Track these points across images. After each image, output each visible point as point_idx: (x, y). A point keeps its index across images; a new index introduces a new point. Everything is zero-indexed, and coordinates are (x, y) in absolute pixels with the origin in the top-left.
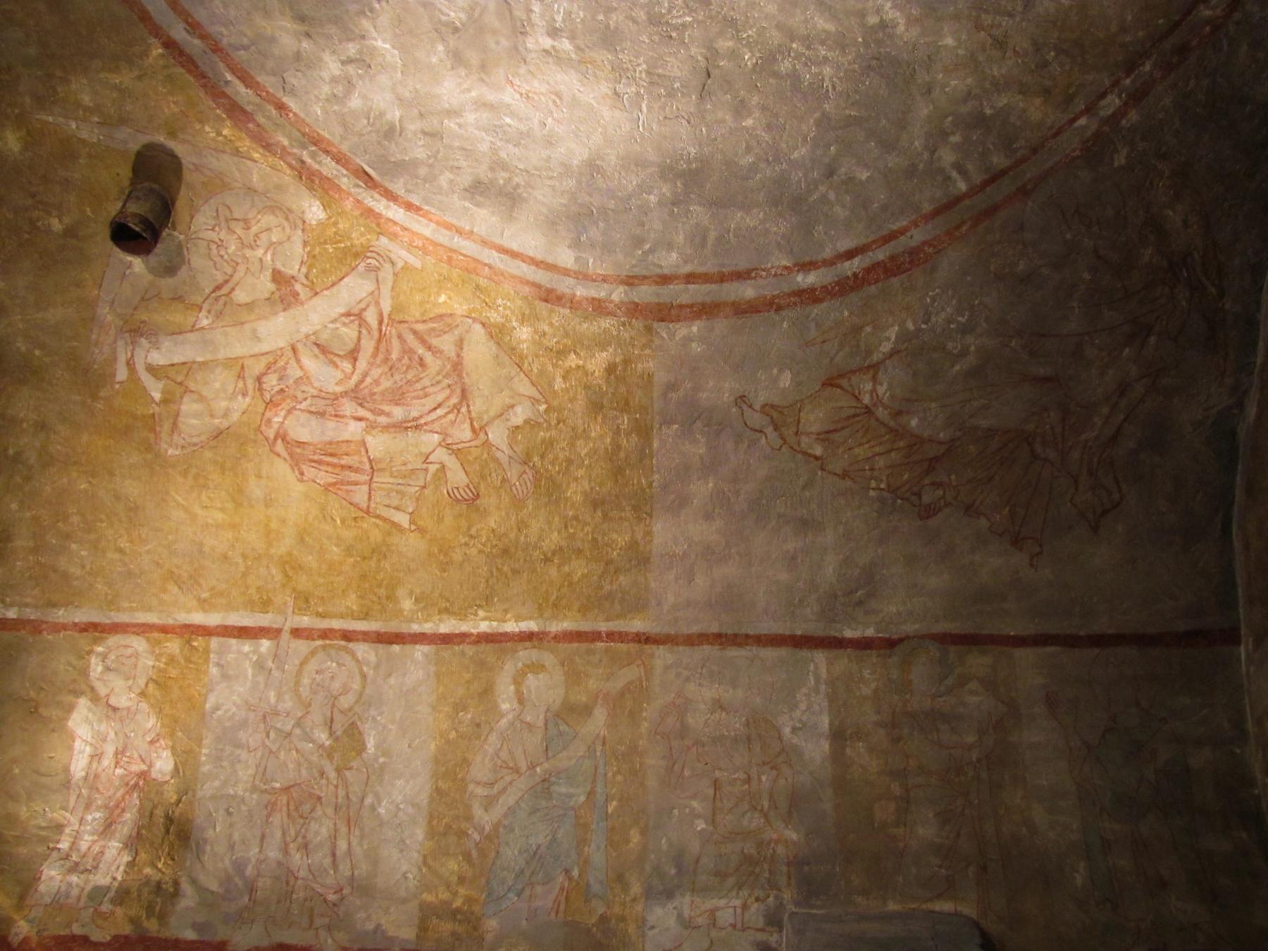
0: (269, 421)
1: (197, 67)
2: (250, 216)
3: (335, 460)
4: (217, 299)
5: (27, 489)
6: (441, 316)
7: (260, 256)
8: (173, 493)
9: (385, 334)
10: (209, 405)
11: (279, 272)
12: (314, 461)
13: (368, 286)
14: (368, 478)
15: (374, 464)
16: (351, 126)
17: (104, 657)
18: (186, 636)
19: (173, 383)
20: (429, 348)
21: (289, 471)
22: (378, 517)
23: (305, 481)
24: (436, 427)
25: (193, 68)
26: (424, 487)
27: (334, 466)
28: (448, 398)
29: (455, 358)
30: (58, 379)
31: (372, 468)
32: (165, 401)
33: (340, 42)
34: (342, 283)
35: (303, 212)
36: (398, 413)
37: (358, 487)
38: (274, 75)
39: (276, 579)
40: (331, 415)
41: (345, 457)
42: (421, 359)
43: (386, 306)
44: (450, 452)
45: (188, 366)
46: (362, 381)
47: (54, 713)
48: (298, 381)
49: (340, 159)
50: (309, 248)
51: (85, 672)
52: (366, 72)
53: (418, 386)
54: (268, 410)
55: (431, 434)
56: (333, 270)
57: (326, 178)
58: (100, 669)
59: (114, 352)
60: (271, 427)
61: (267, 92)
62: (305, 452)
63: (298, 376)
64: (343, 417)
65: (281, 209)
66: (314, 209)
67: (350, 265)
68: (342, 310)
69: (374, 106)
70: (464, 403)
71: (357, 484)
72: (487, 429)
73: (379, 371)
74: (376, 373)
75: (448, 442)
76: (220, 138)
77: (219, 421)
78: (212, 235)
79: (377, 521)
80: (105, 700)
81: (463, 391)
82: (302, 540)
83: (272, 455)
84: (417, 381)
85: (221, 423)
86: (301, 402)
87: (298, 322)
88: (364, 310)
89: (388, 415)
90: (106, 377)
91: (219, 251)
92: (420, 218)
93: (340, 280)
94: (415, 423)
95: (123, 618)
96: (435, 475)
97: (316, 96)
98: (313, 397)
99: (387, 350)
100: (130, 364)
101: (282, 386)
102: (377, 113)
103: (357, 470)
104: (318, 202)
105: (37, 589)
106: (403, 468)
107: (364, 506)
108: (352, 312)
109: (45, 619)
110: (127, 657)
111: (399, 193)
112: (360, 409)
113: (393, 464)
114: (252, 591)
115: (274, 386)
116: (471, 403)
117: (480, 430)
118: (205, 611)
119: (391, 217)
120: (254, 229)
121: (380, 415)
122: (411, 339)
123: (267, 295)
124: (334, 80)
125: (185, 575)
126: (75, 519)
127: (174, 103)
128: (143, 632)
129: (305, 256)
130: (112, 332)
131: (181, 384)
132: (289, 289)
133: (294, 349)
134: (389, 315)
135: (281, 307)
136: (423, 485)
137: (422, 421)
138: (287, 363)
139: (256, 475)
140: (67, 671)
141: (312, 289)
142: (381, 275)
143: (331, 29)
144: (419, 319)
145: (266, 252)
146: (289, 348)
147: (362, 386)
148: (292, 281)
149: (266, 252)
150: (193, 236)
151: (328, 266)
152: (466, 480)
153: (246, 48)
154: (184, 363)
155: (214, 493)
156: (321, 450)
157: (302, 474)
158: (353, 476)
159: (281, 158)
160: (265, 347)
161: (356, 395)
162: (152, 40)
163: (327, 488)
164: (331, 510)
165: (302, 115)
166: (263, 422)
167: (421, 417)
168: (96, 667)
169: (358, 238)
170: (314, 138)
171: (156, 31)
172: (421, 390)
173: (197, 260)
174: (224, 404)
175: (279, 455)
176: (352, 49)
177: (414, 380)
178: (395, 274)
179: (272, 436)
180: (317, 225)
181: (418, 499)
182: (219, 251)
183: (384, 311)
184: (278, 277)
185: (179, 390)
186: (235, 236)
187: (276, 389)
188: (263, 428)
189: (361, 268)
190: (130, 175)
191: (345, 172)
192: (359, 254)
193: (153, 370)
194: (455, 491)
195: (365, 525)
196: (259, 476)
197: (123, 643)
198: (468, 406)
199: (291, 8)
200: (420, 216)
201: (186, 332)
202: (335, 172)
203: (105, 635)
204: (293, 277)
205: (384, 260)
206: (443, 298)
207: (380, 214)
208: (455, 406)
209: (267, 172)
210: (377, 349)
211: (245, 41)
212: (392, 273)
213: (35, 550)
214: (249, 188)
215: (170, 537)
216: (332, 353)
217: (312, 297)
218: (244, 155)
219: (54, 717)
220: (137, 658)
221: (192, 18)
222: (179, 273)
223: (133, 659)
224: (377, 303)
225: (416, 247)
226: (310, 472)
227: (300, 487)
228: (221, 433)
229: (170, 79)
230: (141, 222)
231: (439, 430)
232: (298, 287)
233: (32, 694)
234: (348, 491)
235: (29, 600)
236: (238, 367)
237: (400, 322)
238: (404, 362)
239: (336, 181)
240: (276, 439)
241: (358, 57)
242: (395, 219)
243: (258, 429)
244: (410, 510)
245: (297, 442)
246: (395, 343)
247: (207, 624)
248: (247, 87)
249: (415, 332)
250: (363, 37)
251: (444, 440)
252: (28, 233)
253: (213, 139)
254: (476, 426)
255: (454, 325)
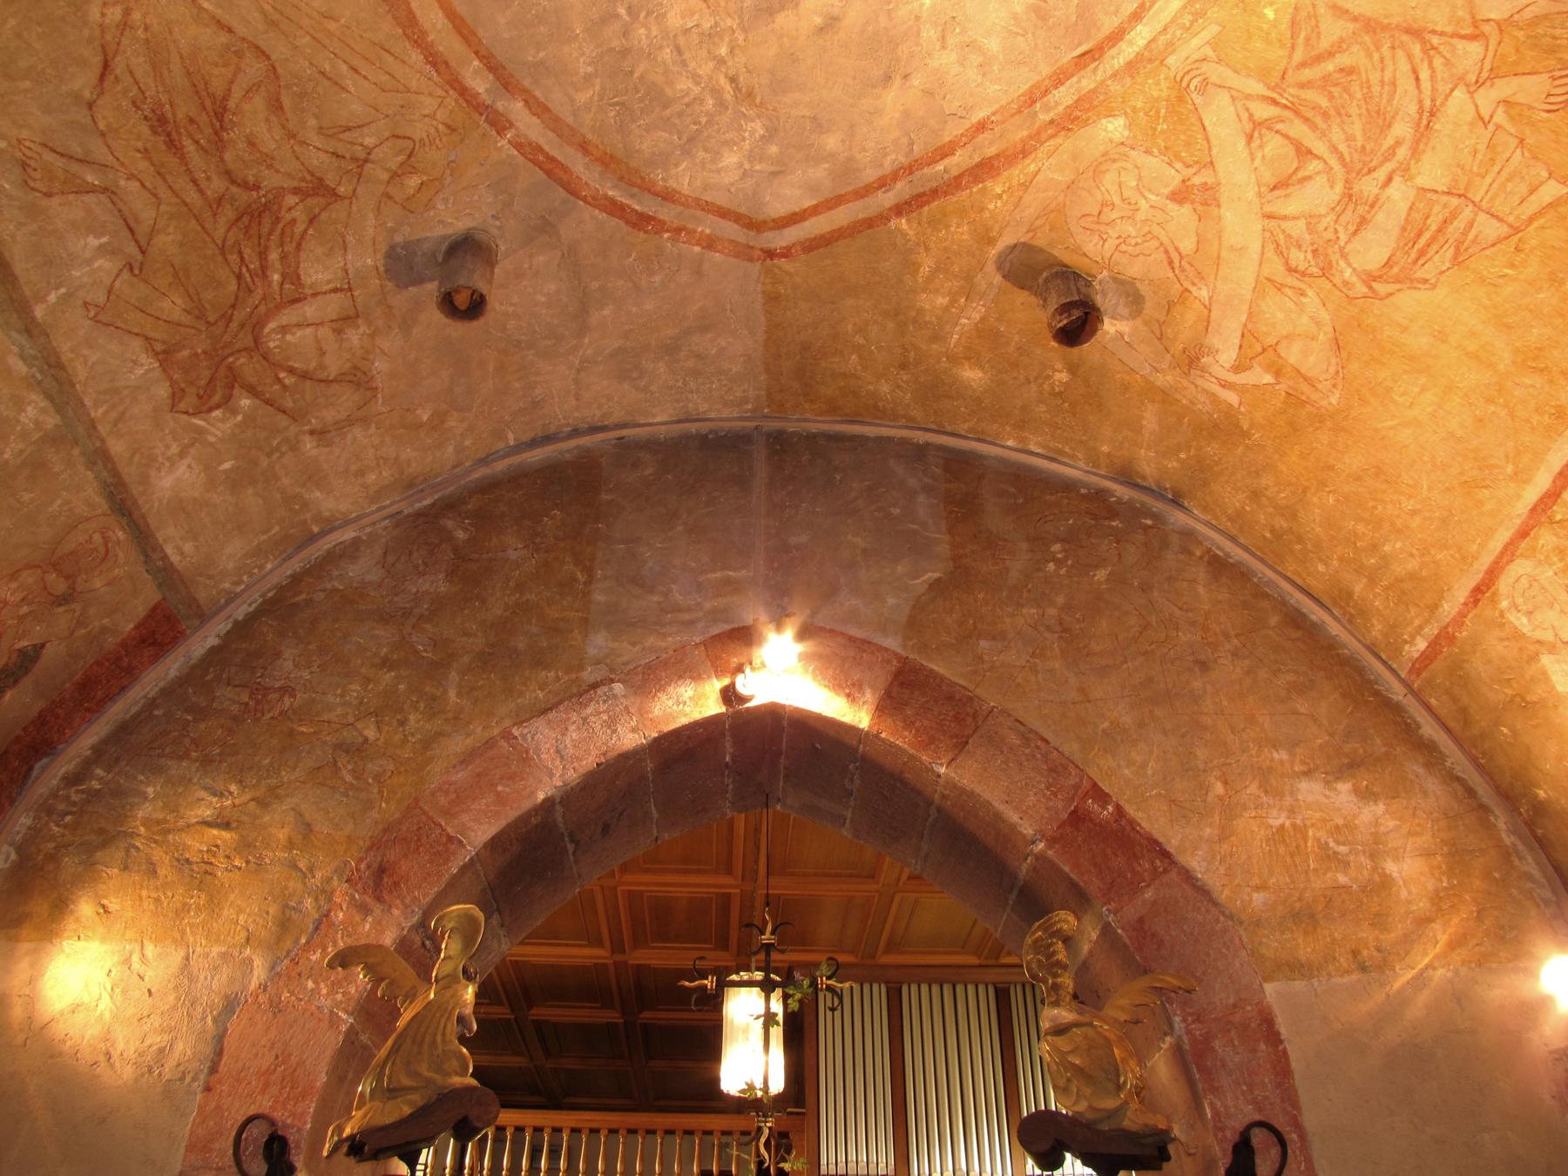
0: (1346, 283)
1: (924, 194)
2: (1100, 198)
3: (1427, 236)
4: (1183, 271)
5: (1309, 546)
6: (1293, 23)
7: (1147, 206)
8: (1379, 426)
9: (1291, 102)
10: (1299, 335)
11: (1173, 193)
12: (1417, 260)
13: (1223, 99)
14: (1471, 207)
15: (1455, 191)
16: (1022, 56)
17: (1516, 607)
18: (1543, 520)
19: (1260, 357)
20: (1330, 54)
21: (1415, 294)
22: (1531, 220)
23: (1436, 282)
24: (1443, 88)
25: (925, 199)
26: (1522, 141)
27: (1434, 239)
28: (1410, 57)
29: (1358, 25)
30: (1215, 454)
31: (1460, 196)
32: (1278, 374)
33: (918, 44)
34: (1209, 128)
35: (1111, 141)
36: (1402, 129)
37: (1476, 224)
38: (945, 122)
39: (1538, 386)
40: (1369, 212)
41: (1429, 222)
42: (1342, 70)
43: (1255, 87)
44: (1488, 83)
45: (1246, 331)
46: (1341, 157)
47: (1539, 692)
48: (1311, 228)
49: (1059, 78)
50: (1155, 151)
51: (1517, 635)
52: (958, 24)
53: (1376, 89)
54: (1331, 278)
55: (1450, 99)
56: (1189, 133)
57: (1076, 102)
58: (1525, 620)
59: (1205, 391)
60: (1354, 285)
61: (962, 135)
62: (1402, 263)
63: (1304, 226)
64: (1377, 199)
65: (1100, 163)
66: (1110, 127)
67: (1190, 111)
68: (1242, 142)
69: (1003, 24)
70: (1427, 36)
71: (1471, 225)
72: (1479, 17)
73: (1336, 129)
74: (1337, 135)
75: (1473, 81)
76: (1004, 197)
77: (1322, 334)
78: (1110, 245)
79: (1536, 224)
80: (1559, 642)
81: (1408, 31)
82: (1509, 327)
83: (1386, 301)
84: (1369, 87)
85: (1325, 334)
86: (1338, 238)
87: (1239, 198)
88: (1251, 116)
89: (1398, 143)
90: (1229, 413)
91: (1130, 245)
92: (1156, 6)
93: (1204, 129)
94: (1426, 115)
95: (1486, 560)
96: (1512, 119)
97: (978, 86)
98: (1336, 222)
99: (1314, 108)
100: (1225, 385)
101: (1309, 250)
102: (1012, 22)
103: (1454, 215)
104: (1104, 121)
105: (1410, 607)
106: (1479, 156)
107: (1505, 230)
108: (1248, 131)
109: (1444, 624)
110: (1529, 588)
111: (1116, 25)
112: (1375, 175)
113: (1467, 168)
114: (1535, 419)
115: (1306, 257)
116: (1430, 26)
117: (1476, 27)
118: (1528, 481)
119: (1145, 42)
120: (1116, 199)
121: (1394, 154)
122: (1307, 74)
123: (1196, 217)
124: (962, 62)
125: (1475, 472)
126: (1361, 528)
127: (958, 228)
128: (1513, 555)
129: (1162, 157)
130: (1185, 383)
131: (1264, 350)
132: (1196, 191)
133: (1270, 217)
134: (1269, 88)
135: (1213, 209)
136: (1517, 141)
137: (1428, 103)
138: (1284, 232)
139: (1402, 332)
140: (1506, 647)
141: (1205, 166)
142: (1214, 79)
143: (903, 51)
144: (1287, 54)
145: (1146, 198)
146: (1267, 221)
147: (1348, 160)
148: (1188, 183)
149: (1146, 198)
150: (1107, 262)
151: (1183, 137)
152: (1545, 77)
153: (911, 143)
154: (1243, 335)
155: (1400, 386)
156: (1406, 245)
157: (1426, 281)
158: (1459, 224)
159: (1042, 143)
160: (1255, 247)
161: (1356, 169)
162: (892, 224)
163: (1457, 261)
164: (1489, 272)
165: (996, 107)
166: (1344, 290)
167: (1420, 102)
168: (1522, 622)
169: (1158, 88)
170: (1026, 101)
171: (882, 218)
172: (1382, 87)
173: (1134, 270)
174: (1305, 320)
175: (1391, 294)
176: (929, 33)
177: (1365, 91)
178: (1220, 61)
179: (1365, 290)
180: (1130, 130)
181: (1535, 158)
182: (1130, 245)
183: (1260, 93)
184: (1180, 196)
185: (1270, 354)
186: (1118, 221)
187: (1309, 256)
188: (1351, 294)
189: (1198, 100)
190: (1026, 293)
191: (1075, 79)
192: (1180, 92)
193: (1238, 368)
194: (1551, 99)
195: (1534, 242)
196: (1405, 330)
197: (1511, 580)
198: (1434, 32)
199: (874, 87)
200: (1150, 7)
201: (1209, 316)
202: (1072, 91)
203: (1493, 589)
204: (1183, 181)
205: (1197, 69)
206: (1269, 13)
207: (1138, 54)
208: (1425, 52)
209: (1054, 163)
210: (1307, 120)
211: (905, 140)
212: (1216, 66)
213: (1372, 582)
214: (1068, 188)
215: (1426, 459)
216: (1290, 177)
217: (1214, 171)
218: (1029, 180)
219: (1544, 695)
220: (1536, 580)
221: (873, 183)
222: (1143, 293)
223: (1535, 584)
224: (1248, 97)
225: (1192, 24)
226: (1427, 271)
227: (1441, 292)
228: (1336, 339)
229: (934, 223)
230: (1061, 314)
231: (1450, 86)
232: (1197, 180)
233: (1509, 691)
234: (1475, 241)
235: (1417, 622)
236: (1265, 284)
237: (1283, 78)
238: (1336, 94)
239: (1083, 93)
240: (1370, 288)
241: (940, 29)
242: (1149, 39)
243: (1351, 299)
244: (1545, 174)
245: (1383, 266)
246: (1309, 95)
247: (1544, 490)
248: (953, 154)
249: (1303, 65)
250: (918, 18)
251: (1467, 85)
252: (1064, 402)
253: (1005, 204)
254: (1468, 31)
255: (1311, 9)
